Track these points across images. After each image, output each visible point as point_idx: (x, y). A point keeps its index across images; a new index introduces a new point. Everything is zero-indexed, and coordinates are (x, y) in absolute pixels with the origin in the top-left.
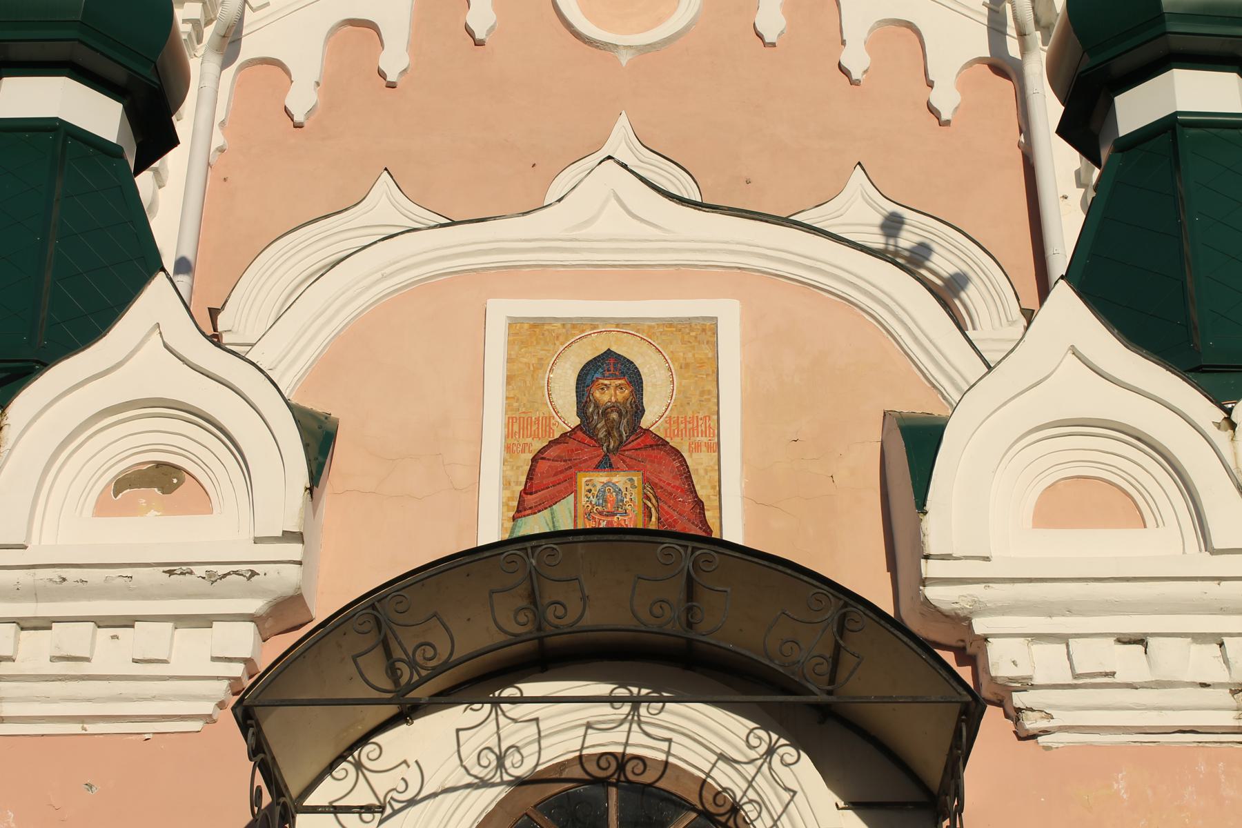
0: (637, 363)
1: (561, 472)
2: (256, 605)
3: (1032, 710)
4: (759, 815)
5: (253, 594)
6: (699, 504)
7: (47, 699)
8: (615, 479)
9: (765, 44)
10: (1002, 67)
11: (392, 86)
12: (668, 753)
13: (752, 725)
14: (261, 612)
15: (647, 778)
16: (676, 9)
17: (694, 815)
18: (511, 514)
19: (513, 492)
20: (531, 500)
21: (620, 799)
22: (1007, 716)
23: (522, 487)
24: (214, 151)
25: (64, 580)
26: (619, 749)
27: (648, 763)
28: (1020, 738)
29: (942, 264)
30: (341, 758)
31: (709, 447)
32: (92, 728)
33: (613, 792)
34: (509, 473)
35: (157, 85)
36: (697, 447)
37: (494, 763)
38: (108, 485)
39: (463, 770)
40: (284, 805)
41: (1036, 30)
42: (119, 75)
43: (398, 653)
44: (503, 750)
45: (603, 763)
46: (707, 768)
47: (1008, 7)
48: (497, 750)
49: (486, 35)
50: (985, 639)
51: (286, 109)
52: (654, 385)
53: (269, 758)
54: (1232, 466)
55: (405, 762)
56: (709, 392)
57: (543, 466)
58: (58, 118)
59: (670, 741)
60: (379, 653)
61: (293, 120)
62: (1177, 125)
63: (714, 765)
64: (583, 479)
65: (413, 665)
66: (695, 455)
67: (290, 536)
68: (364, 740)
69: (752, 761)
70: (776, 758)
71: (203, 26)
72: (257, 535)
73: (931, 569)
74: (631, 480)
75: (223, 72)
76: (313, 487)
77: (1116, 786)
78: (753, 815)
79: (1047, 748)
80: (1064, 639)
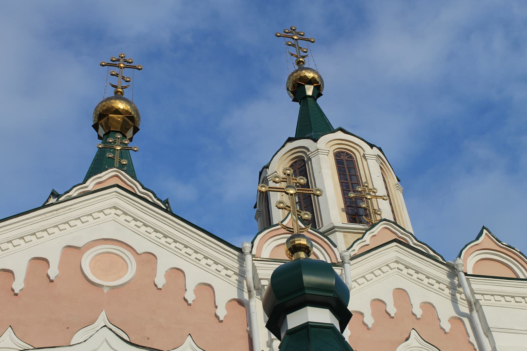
11: (16, 295)
16: (126, 274)
41: (254, 290)
62: (309, 326)
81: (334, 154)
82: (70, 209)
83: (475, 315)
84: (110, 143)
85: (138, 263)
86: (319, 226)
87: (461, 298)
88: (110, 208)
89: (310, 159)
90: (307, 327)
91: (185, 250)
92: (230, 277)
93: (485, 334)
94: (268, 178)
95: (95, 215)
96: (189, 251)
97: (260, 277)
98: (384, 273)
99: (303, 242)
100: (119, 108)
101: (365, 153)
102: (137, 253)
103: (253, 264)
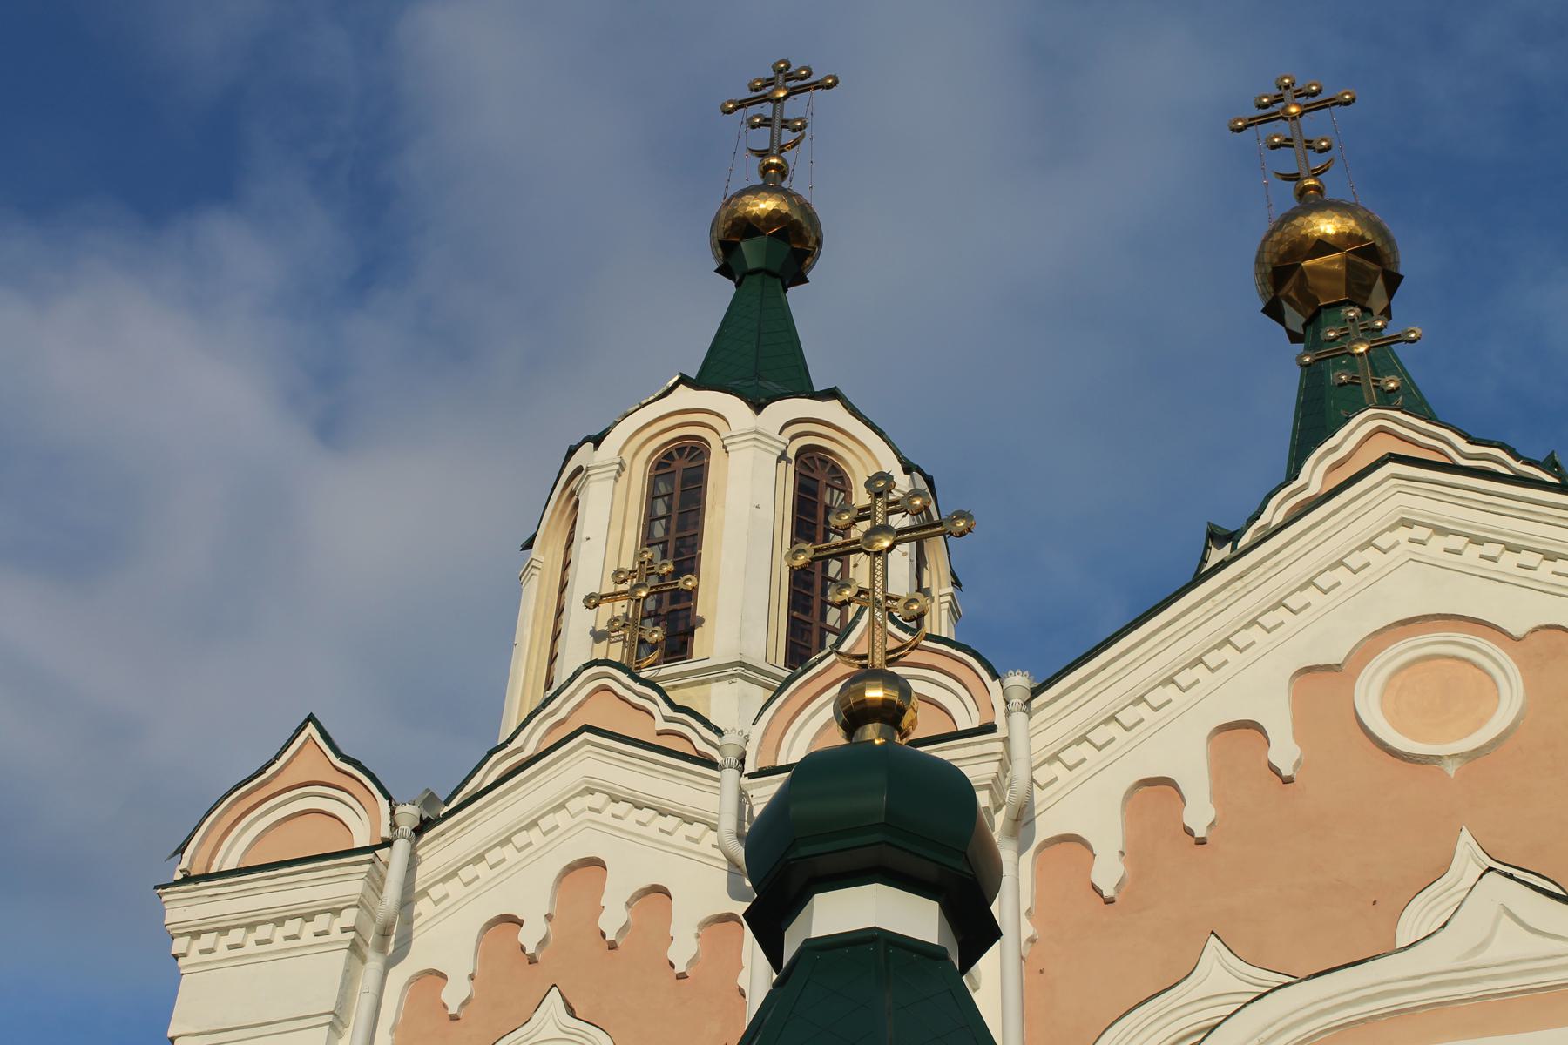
11: (1201, 842)
16: (1497, 706)
24: (1026, 943)
35: (971, 876)
49: (1294, 771)
51: (1094, 887)
58: (875, 928)
61: (1102, 896)
71: (993, 813)
75: (1021, 857)
84: (1333, 340)
88: (1392, 528)
100: (1326, 235)
102: (1511, 637)
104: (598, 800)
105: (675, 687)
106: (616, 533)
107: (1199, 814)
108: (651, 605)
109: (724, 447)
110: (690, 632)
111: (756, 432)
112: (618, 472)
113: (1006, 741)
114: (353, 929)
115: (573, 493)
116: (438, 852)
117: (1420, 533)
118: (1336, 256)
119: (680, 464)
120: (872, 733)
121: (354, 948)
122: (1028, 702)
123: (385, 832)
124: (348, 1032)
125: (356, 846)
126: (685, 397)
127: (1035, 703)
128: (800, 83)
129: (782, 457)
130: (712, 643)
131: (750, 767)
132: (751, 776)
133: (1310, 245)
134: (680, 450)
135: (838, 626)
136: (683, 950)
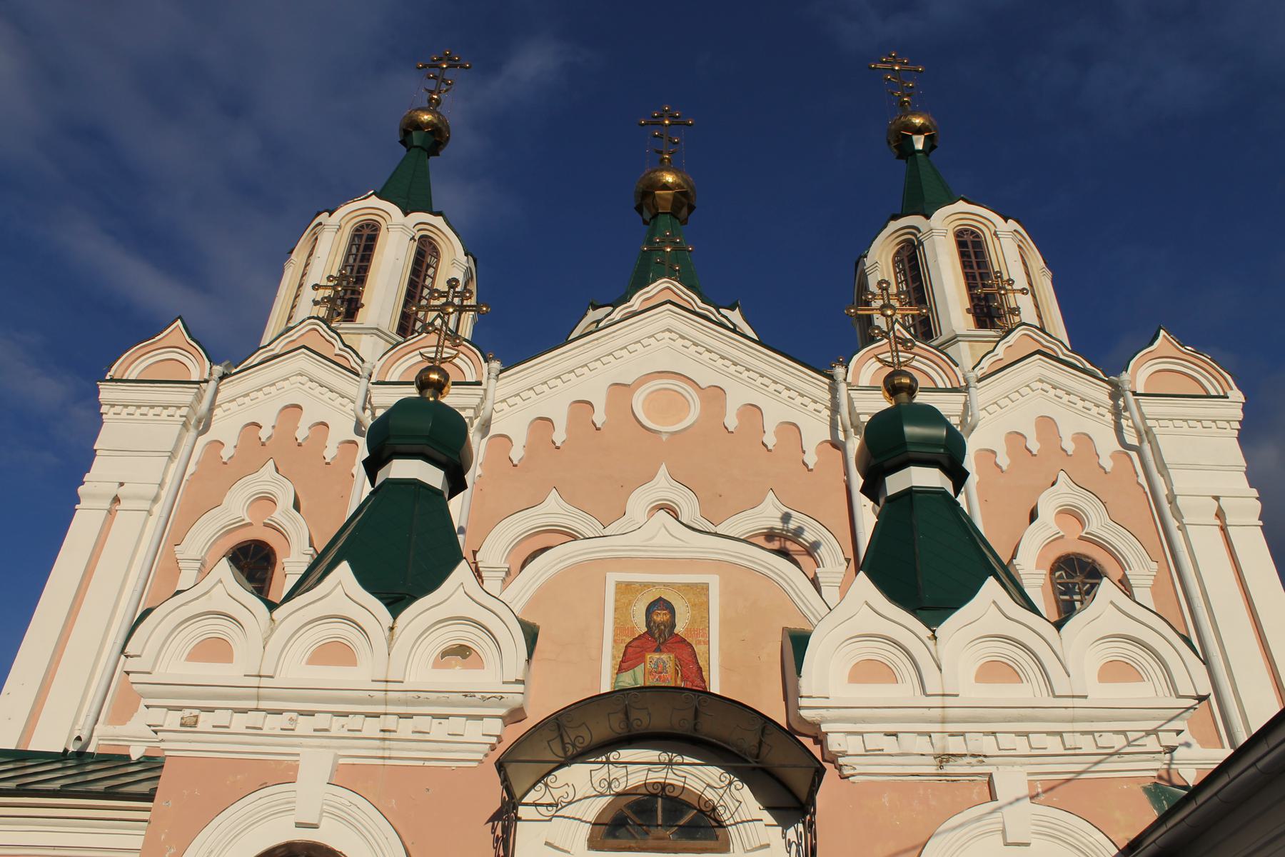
0: (673, 603)
1: (639, 653)
2: (502, 712)
3: (847, 766)
4: (725, 812)
5: (502, 706)
6: (700, 669)
7: (410, 750)
8: (662, 657)
9: (729, 432)
10: (836, 445)
11: (558, 448)
12: (685, 783)
13: (723, 771)
14: (505, 715)
15: (675, 794)
16: (688, 415)
17: (695, 811)
18: (616, 671)
19: (617, 661)
20: (624, 665)
21: (663, 803)
22: (836, 768)
23: (620, 659)
25: (419, 697)
26: (663, 781)
27: (676, 787)
28: (841, 778)
29: (809, 536)
30: (539, 781)
31: (705, 643)
32: (427, 764)
33: (660, 800)
34: (615, 653)
36: (699, 643)
37: (607, 786)
38: (438, 654)
39: (592, 789)
40: (514, 804)
42: (443, 458)
43: (567, 740)
44: (611, 780)
45: (655, 787)
46: (702, 790)
47: (839, 417)
48: (608, 780)
49: (602, 425)
50: (826, 733)
52: (680, 614)
53: (509, 784)
54: (935, 655)
55: (567, 784)
56: (705, 617)
57: (630, 649)
59: (685, 777)
60: (558, 740)
63: (705, 789)
64: (648, 656)
65: (574, 746)
66: (698, 646)
67: (518, 682)
68: (549, 774)
69: (722, 788)
70: (733, 786)
72: (504, 680)
73: (802, 702)
74: (670, 657)
76: (529, 661)
77: (883, 800)
78: (722, 812)
79: (854, 783)
80: (861, 734)
81: (954, 234)
82: (613, 337)
83: (1147, 447)
84: (658, 243)
85: (702, 400)
86: (936, 335)
87: (1128, 426)
88: (663, 332)
89: (921, 243)
90: (910, 493)
91: (760, 380)
92: (819, 412)
93: (1159, 472)
94: (866, 271)
95: (645, 342)
96: (765, 381)
97: (858, 411)
98: (1023, 396)
99: (906, 381)
100: (668, 182)
101: (997, 230)
102: (700, 387)
103: (849, 395)
104: (304, 379)
105: (346, 333)
106: (331, 258)
107: (559, 436)
108: (341, 294)
109: (388, 229)
110: (357, 309)
111: (403, 225)
112: (338, 230)
113: (485, 390)
114: (185, 416)
115: (315, 234)
116: (228, 389)
117: (674, 336)
118: (671, 192)
119: (366, 232)
120: (429, 394)
121: (185, 425)
122: (497, 375)
123: (206, 376)
124: (177, 461)
125: (192, 380)
126: (374, 201)
127: (501, 376)
128: (454, 63)
129: (413, 238)
130: (366, 316)
131: (373, 380)
132: (373, 384)
133: (660, 185)
134: (368, 225)
135: (422, 318)
136: (330, 452)
